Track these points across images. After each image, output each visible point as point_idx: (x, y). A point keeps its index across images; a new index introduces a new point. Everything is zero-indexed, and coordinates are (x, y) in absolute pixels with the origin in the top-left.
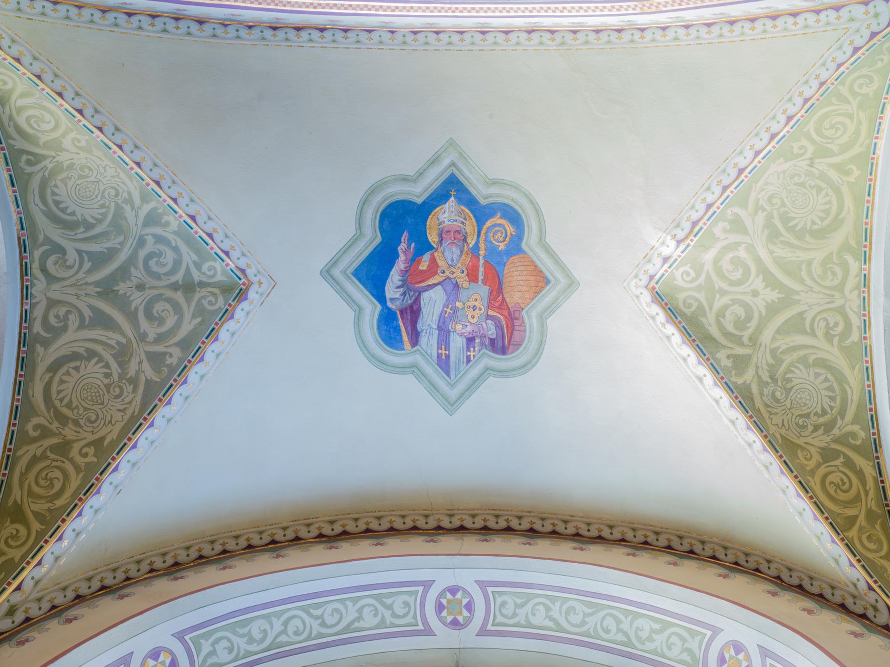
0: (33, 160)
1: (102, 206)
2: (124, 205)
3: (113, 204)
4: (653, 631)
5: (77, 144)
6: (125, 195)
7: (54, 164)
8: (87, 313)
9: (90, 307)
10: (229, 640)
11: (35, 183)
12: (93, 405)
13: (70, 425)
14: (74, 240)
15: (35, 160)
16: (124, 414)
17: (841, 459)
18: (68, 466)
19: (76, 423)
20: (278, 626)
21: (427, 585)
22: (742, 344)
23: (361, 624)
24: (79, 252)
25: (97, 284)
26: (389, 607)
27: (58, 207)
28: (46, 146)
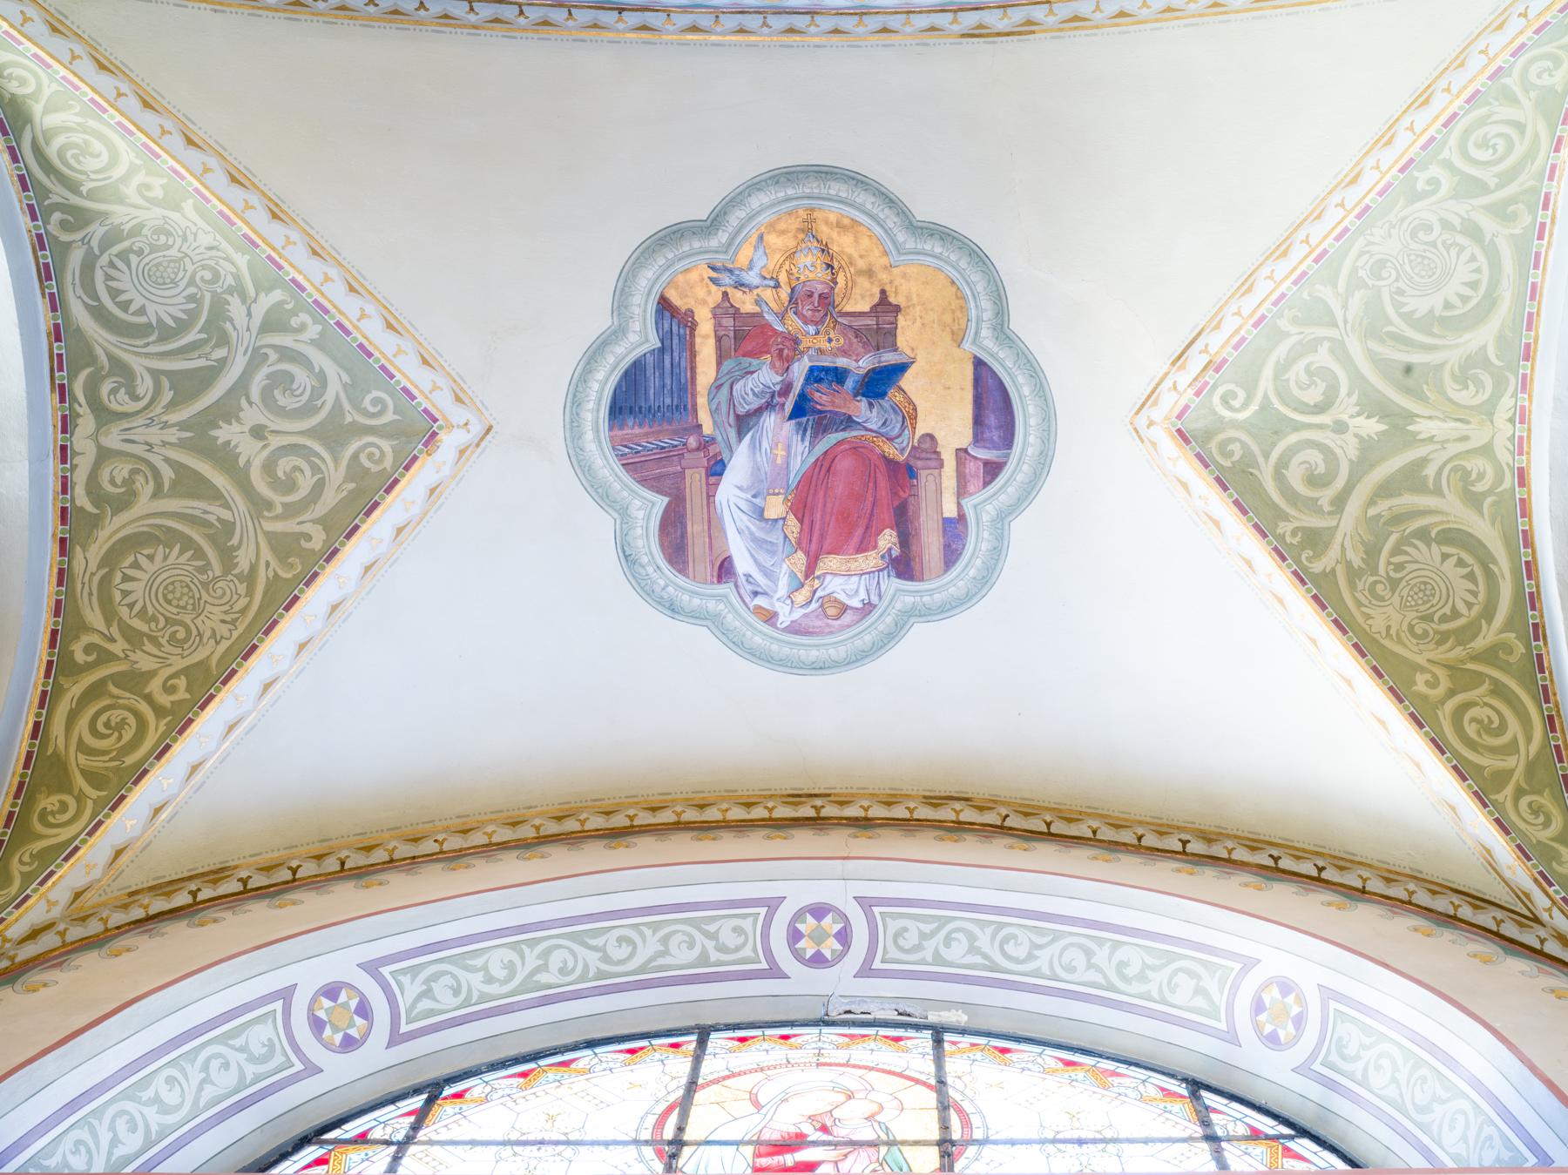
0: (72, 220)
1: (191, 298)
2: (229, 298)
3: (208, 296)
4: (1145, 966)
5: (146, 193)
6: (230, 281)
7: (107, 228)
8: (168, 473)
9: (167, 460)
10: (454, 977)
11: (76, 258)
12: (178, 613)
13: (1457, 222)
14: (147, 355)
15: (79, 218)
16: (233, 627)
17: (1486, 686)
18: (144, 707)
19: (154, 640)
20: (532, 960)
21: (773, 904)
22: (1319, 511)
23: (668, 960)
24: (156, 374)
25: (183, 426)
26: (713, 936)
27: (113, 299)
28: (91, 195)
